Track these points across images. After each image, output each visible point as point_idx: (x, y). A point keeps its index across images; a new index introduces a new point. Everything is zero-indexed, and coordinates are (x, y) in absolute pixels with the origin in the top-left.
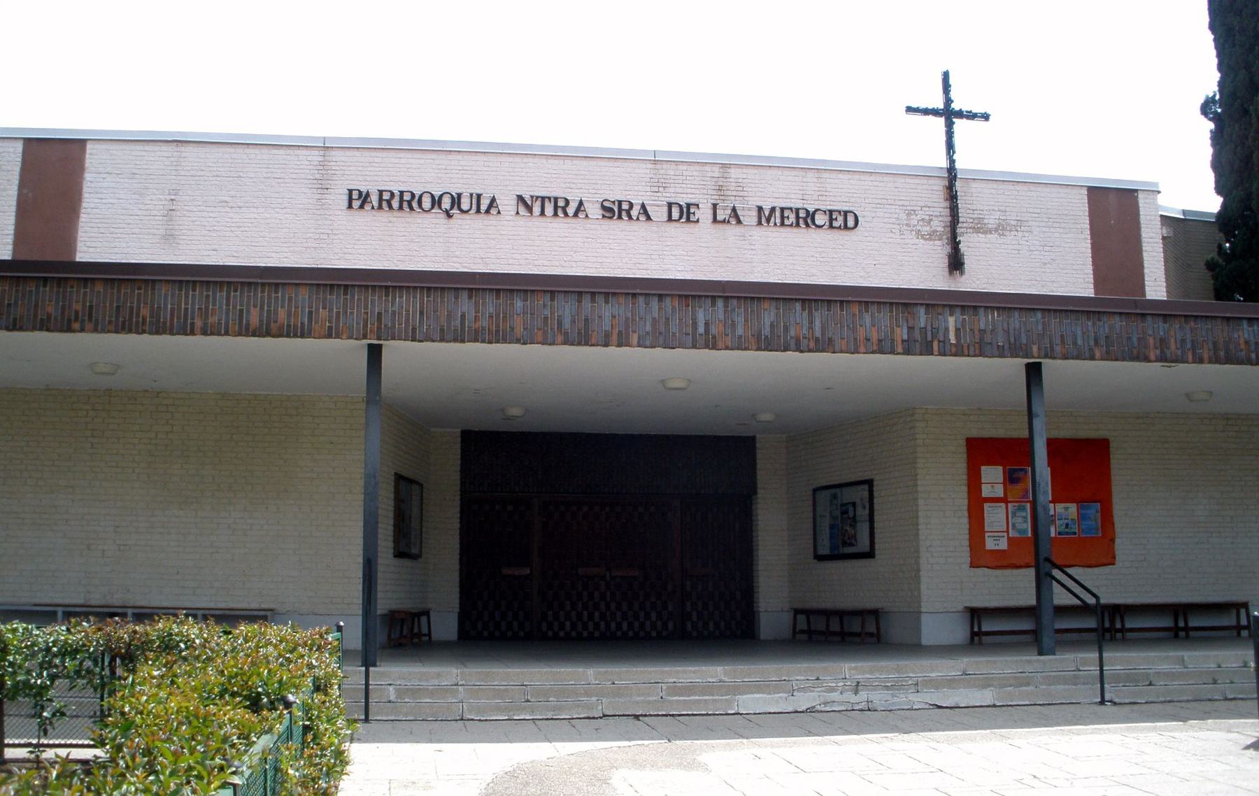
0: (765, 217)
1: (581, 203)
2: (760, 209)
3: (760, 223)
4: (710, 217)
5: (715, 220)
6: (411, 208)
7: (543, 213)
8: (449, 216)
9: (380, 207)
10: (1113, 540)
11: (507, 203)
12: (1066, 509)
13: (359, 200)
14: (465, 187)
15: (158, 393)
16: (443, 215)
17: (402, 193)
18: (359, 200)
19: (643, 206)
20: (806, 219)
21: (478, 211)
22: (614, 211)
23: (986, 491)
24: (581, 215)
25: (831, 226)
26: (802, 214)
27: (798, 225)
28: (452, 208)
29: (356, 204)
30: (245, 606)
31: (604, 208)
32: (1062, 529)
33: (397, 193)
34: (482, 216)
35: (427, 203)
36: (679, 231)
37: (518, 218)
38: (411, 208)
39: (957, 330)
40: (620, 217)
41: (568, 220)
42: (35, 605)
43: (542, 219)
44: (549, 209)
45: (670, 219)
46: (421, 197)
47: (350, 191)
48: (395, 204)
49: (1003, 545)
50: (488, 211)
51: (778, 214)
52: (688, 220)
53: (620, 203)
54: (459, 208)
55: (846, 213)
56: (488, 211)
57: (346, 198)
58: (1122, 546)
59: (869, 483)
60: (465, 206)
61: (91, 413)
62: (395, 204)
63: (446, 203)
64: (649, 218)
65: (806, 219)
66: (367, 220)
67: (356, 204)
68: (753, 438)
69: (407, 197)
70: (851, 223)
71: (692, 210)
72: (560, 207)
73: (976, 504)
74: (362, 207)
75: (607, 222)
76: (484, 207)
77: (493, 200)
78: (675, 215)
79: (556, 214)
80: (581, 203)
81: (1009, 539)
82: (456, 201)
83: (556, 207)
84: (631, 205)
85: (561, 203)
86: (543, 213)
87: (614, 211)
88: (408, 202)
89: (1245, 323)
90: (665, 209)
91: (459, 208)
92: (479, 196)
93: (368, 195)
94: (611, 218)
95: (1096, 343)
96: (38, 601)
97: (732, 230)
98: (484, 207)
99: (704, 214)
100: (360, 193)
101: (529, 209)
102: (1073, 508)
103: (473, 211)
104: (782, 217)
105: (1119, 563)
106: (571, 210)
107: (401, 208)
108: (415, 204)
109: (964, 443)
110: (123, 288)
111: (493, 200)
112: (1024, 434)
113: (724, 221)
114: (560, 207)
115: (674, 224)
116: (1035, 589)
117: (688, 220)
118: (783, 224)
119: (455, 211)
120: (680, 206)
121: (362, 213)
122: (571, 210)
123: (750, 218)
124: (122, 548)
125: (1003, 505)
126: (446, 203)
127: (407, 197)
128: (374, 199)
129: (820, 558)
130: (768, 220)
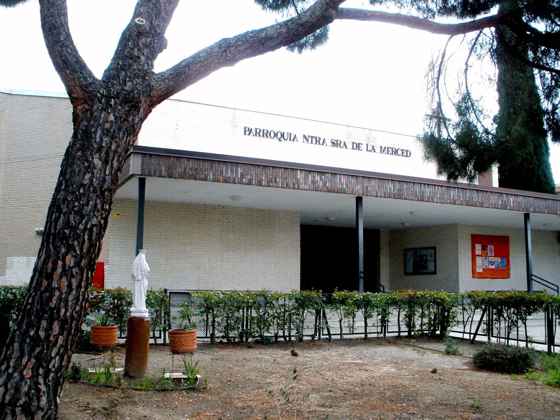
0: (383, 150)
1: (324, 140)
2: (381, 147)
3: (381, 152)
4: (366, 149)
5: (367, 150)
6: (267, 136)
7: (312, 142)
8: (280, 141)
9: (256, 135)
10: (509, 270)
11: (300, 138)
12: (498, 259)
13: (248, 131)
14: (286, 131)
15: (224, 207)
16: (278, 141)
17: (264, 130)
18: (248, 131)
19: (344, 143)
20: (395, 152)
21: (290, 140)
22: (335, 144)
23: (477, 253)
24: (325, 144)
25: (403, 156)
26: (394, 150)
27: (256, 135)
28: (281, 138)
29: (247, 133)
30: (178, 289)
31: (332, 143)
32: (497, 266)
33: (262, 130)
34: (291, 142)
35: (272, 135)
36: (356, 152)
37: (303, 143)
38: (267, 136)
39: (513, 202)
40: (337, 146)
41: (320, 146)
42: (186, 290)
43: (312, 145)
44: (314, 140)
45: (353, 148)
46: (270, 132)
47: (245, 128)
48: (261, 134)
49: (481, 271)
50: (293, 140)
51: (386, 149)
52: (359, 149)
53: (337, 141)
54: (284, 138)
55: (407, 151)
56: (293, 140)
57: (243, 130)
58: (512, 272)
59: (434, 248)
60: (286, 138)
61: (198, 214)
62: (261, 134)
63: (279, 136)
64: (346, 148)
65: (395, 152)
66: (251, 138)
67: (247, 133)
68: (379, 230)
69: (265, 132)
70: (408, 155)
71: (360, 146)
72: (318, 141)
73: (474, 257)
74: (249, 134)
75: (333, 147)
76: (292, 138)
77: (295, 136)
78: (355, 147)
79: (316, 143)
80: (324, 140)
81: (483, 269)
82: (397, 151)
83: (316, 140)
84: (341, 142)
85: (318, 139)
86: (312, 142)
87: (335, 144)
88: (266, 134)
89: (271, 168)
90: (351, 144)
91: (284, 138)
92: (290, 134)
93: (251, 130)
94: (334, 146)
95: (546, 208)
96: (186, 289)
97: (372, 153)
98: (292, 138)
99: (363, 147)
100: (249, 129)
101: (307, 140)
102: (499, 259)
103: (289, 139)
104: (388, 151)
105: (511, 278)
106: (321, 142)
107: (263, 136)
108: (268, 135)
109: (470, 236)
110: (239, 168)
111: (295, 136)
112: (353, 223)
113: (370, 151)
114: (318, 141)
115: (354, 150)
116: (527, 286)
117: (359, 149)
118: (388, 153)
119: (282, 139)
120: (356, 144)
121: (249, 137)
122: (321, 142)
123: (378, 150)
124: (212, 267)
125: (481, 257)
126: (279, 136)
127: (265, 132)
128: (254, 131)
129: (406, 274)
130: (384, 151)
